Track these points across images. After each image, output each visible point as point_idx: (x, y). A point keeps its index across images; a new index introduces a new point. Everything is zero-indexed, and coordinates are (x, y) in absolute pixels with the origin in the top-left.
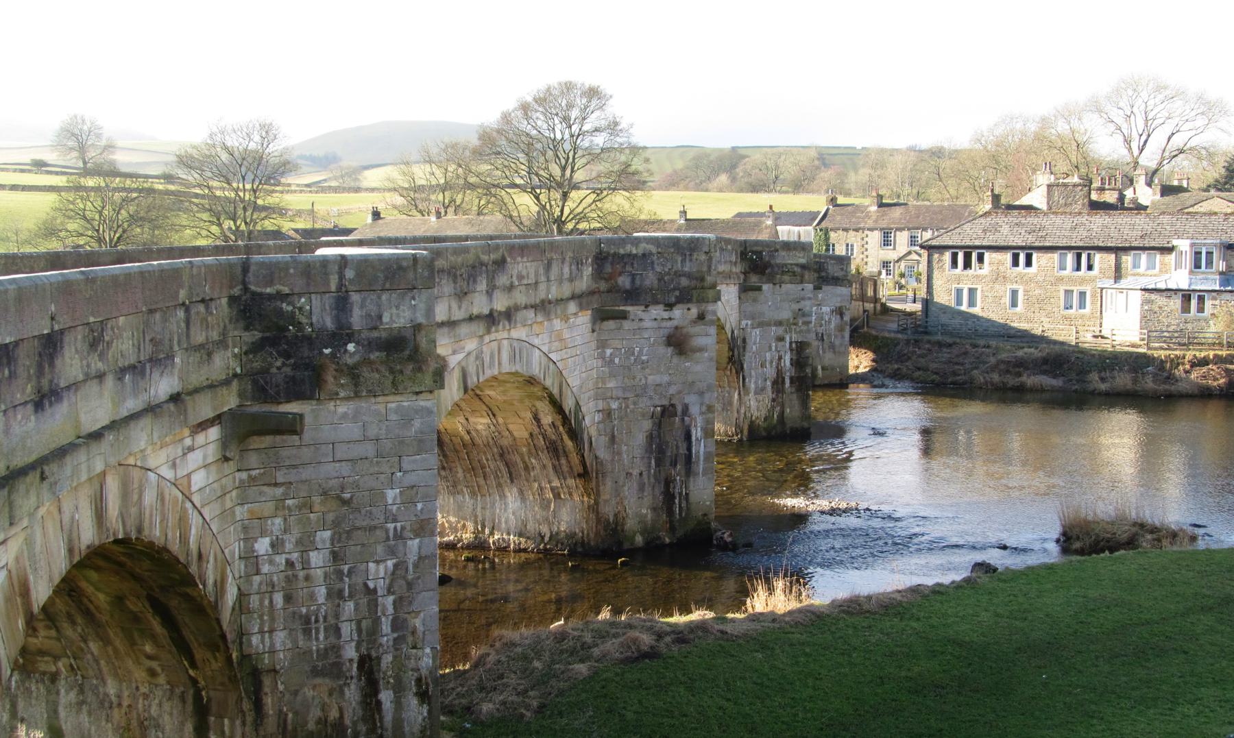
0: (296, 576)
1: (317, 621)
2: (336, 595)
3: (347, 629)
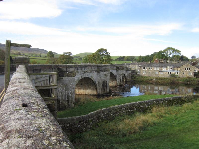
2: (66, 94)
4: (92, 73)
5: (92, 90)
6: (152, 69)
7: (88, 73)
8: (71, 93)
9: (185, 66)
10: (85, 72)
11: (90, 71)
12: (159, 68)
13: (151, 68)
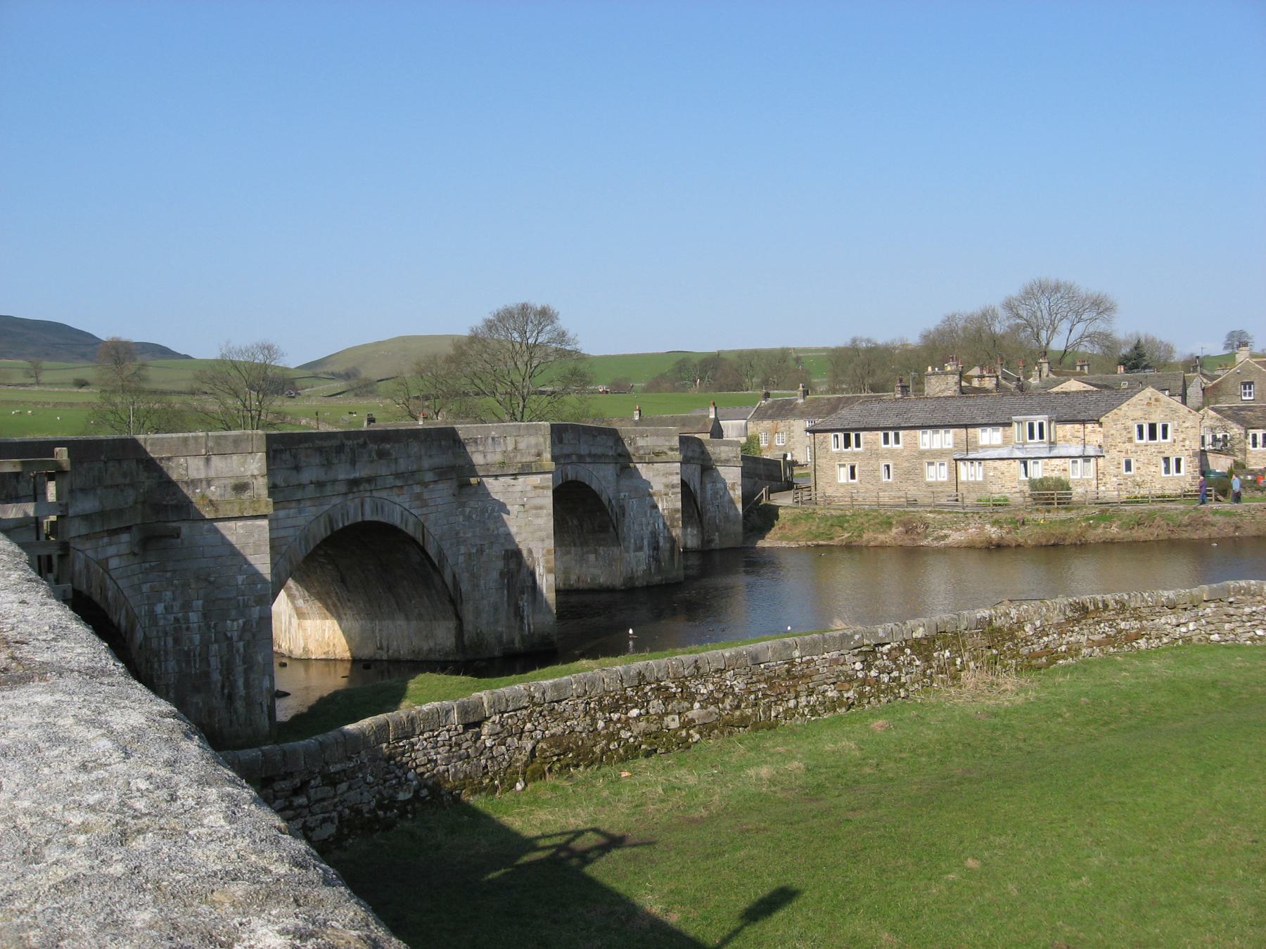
0: (180, 628)
1: (194, 656)
3: (214, 662)
4: (417, 489)
5: (420, 617)
6: (900, 446)
7: (384, 494)
8: (248, 636)
9: (1139, 414)
10: (354, 483)
11: (398, 475)
12: (952, 431)
13: (897, 436)
